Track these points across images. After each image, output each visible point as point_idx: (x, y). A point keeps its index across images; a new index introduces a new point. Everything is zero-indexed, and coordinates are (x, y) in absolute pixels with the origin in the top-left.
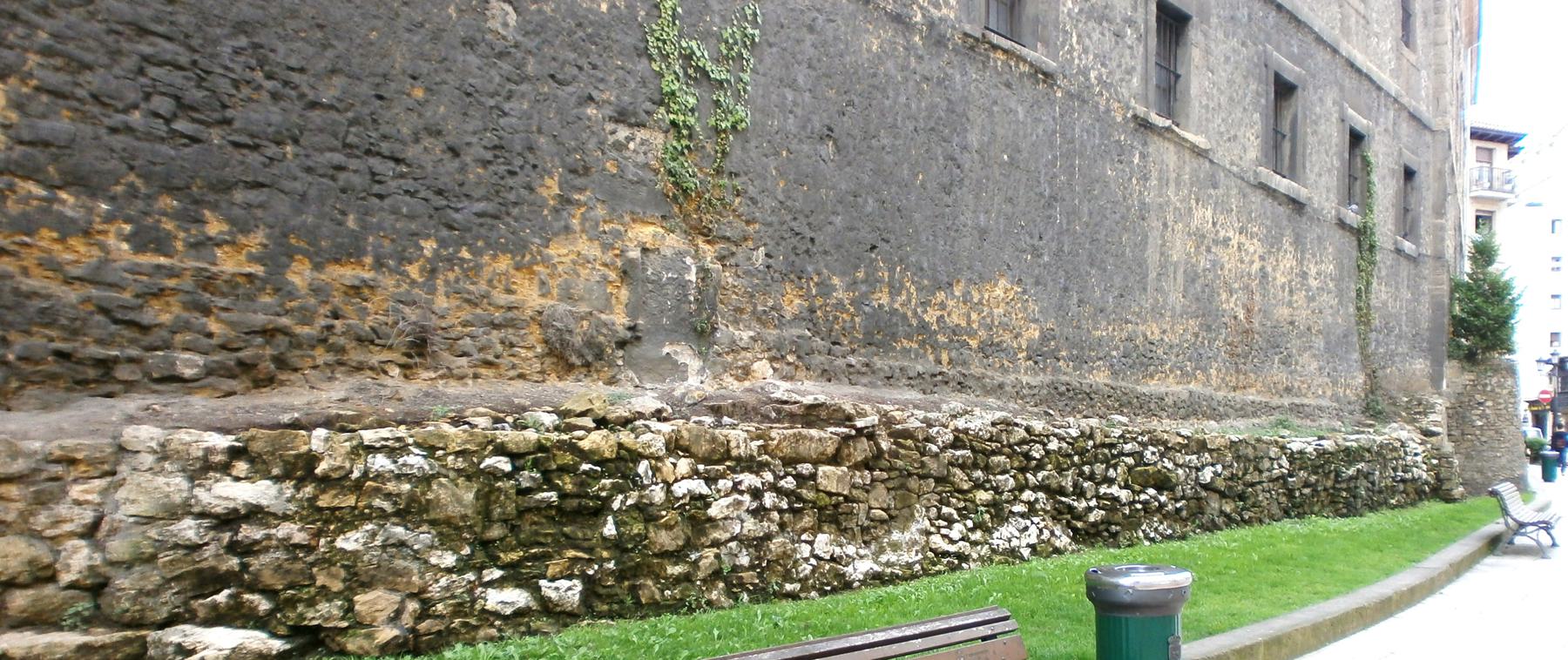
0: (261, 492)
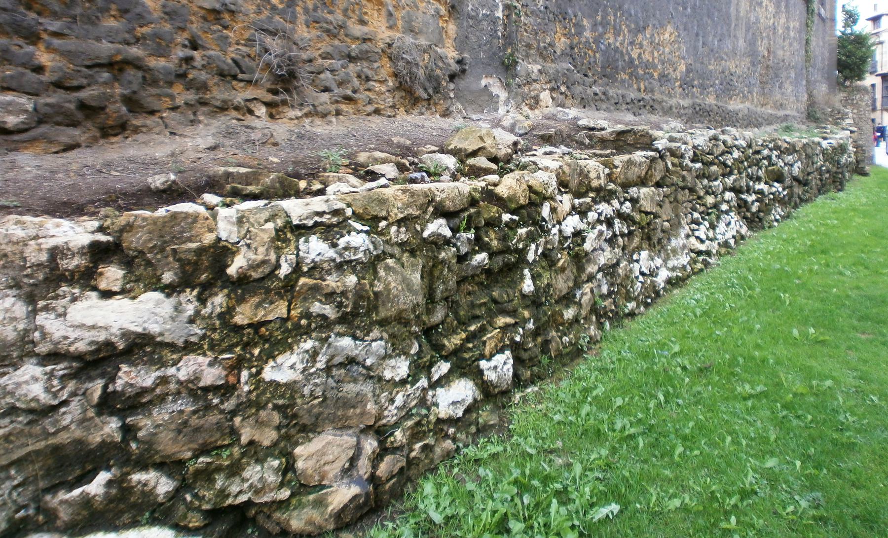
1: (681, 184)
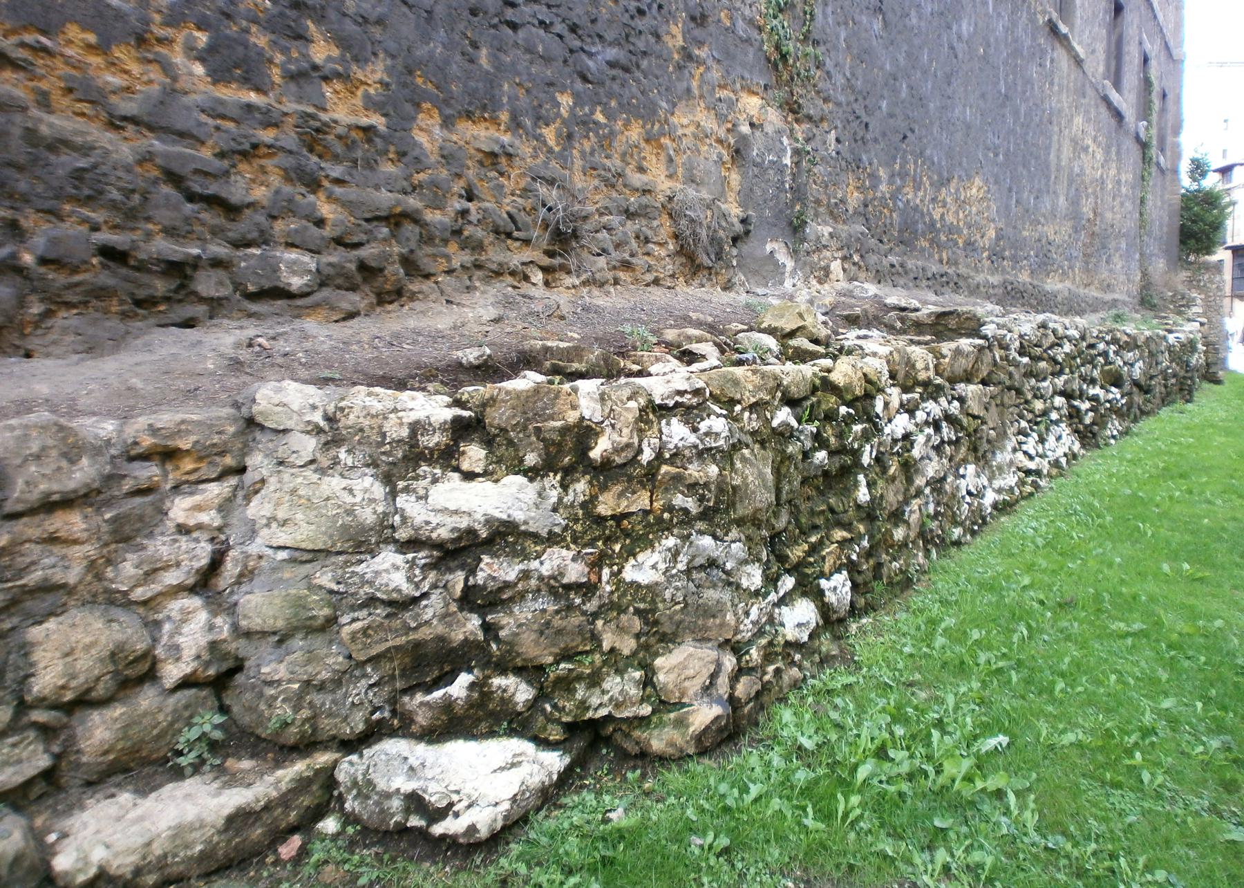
0: (507, 497)
1: (1008, 383)
